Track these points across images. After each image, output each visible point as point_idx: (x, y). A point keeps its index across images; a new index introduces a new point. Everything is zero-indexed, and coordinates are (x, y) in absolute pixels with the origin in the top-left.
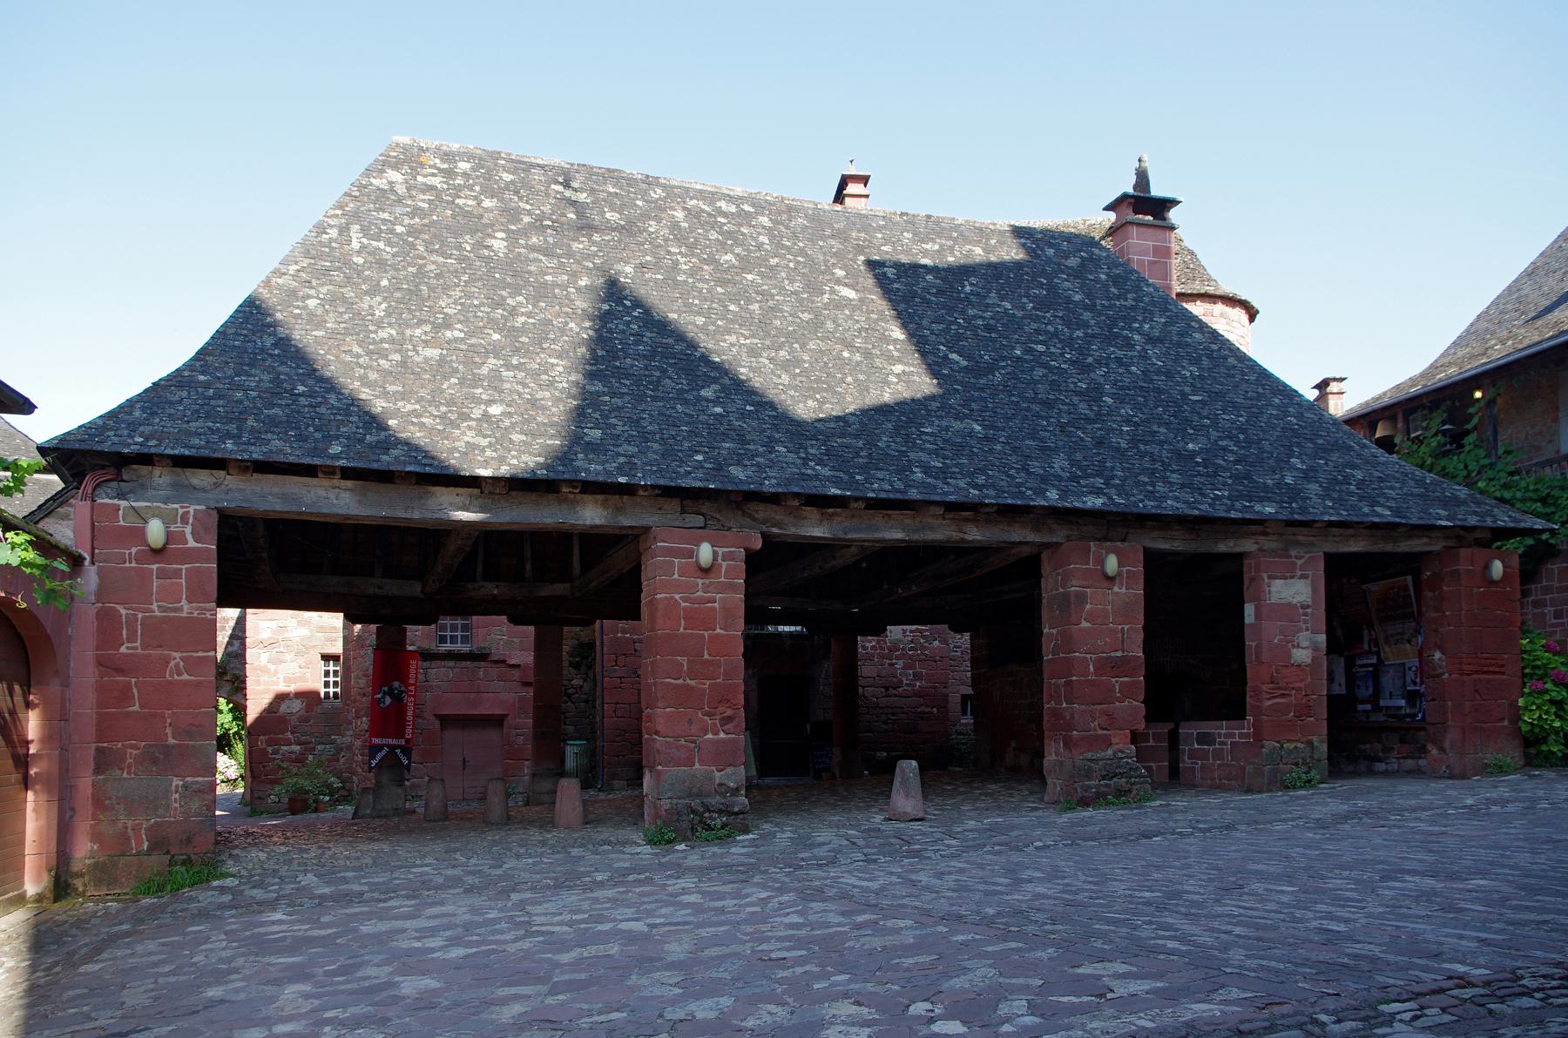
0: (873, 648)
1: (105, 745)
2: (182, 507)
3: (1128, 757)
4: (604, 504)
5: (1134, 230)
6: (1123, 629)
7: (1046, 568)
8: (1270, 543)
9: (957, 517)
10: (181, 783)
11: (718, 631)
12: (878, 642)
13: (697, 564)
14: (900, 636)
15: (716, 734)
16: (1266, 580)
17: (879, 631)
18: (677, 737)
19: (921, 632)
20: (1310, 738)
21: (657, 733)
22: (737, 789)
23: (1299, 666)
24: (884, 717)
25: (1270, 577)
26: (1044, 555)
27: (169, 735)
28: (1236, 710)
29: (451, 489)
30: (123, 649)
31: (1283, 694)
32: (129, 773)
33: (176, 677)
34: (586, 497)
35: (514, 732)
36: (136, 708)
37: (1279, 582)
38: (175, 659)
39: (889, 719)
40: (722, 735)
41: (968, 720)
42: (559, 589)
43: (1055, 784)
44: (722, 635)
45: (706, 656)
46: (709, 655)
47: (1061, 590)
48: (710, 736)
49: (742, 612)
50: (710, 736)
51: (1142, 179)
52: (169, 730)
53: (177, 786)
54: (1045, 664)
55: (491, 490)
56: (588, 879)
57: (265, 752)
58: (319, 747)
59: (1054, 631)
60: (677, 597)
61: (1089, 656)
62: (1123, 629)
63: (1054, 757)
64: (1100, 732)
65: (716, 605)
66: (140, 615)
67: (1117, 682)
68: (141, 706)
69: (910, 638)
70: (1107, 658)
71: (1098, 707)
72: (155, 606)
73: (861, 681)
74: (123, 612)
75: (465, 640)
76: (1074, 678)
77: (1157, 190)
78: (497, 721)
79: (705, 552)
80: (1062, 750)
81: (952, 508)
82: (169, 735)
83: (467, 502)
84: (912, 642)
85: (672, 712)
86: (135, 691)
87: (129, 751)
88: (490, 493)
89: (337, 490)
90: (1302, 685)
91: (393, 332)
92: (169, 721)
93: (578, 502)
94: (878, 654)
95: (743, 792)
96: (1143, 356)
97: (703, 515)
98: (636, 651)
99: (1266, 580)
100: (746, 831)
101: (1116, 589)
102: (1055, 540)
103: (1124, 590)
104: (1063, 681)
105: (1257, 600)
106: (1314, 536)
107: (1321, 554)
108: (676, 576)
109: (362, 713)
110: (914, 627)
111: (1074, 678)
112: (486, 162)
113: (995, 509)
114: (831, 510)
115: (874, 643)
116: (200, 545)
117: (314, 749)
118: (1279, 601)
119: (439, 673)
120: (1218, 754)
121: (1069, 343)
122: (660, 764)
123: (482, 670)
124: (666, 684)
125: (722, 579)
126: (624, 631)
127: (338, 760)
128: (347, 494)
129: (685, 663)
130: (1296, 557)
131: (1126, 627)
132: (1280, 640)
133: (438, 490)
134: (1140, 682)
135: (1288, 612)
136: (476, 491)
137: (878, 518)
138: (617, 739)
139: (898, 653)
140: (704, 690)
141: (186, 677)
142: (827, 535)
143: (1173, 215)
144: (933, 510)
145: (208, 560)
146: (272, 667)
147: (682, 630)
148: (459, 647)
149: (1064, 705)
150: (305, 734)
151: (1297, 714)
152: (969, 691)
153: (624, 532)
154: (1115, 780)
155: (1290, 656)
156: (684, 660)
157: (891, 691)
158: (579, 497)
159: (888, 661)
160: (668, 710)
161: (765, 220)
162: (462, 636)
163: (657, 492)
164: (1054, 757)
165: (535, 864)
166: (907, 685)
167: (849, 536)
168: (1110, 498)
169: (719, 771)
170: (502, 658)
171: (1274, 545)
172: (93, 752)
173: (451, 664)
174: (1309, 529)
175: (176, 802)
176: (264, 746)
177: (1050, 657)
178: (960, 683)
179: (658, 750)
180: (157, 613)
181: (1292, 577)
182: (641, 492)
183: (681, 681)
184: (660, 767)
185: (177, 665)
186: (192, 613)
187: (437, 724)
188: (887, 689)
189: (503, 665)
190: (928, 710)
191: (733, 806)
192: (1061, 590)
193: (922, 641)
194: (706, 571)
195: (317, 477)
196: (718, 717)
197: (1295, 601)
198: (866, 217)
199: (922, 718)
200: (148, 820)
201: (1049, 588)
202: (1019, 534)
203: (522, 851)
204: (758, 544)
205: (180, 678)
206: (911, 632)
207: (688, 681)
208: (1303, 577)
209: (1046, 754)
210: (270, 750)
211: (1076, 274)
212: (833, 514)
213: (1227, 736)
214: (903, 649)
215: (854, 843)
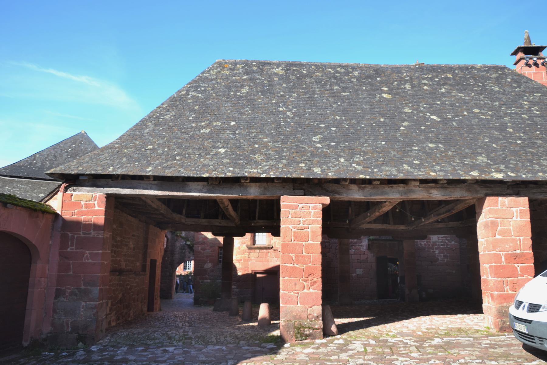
0: (425, 244)
1: (59, 287)
2: (94, 194)
4: (259, 187)
9: (426, 186)
10: (85, 304)
11: (310, 242)
12: (427, 242)
14: (437, 240)
19: (446, 237)
27: (82, 284)
30: (69, 250)
32: (66, 299)
33: (86, 261)
36: (71, 273)
38: (87, 253)
51: (529, 40)
52: (82, 282)
53: (83, 306)
55: (212, 182)
60: (290, 226)
61: (501, 253)
62: (520, 239)
65: (309, 230)
66: (76, 236)
67: (518, 267)
68: (73, 273)
69: (441, 240)
70: (511, 254)
71: (509, 279)
72: (81, 233)
74: (70, 235)
82: (82, 284)
83: (202, 188)
84: (442, 242)
85: (288, 279)
86: (71, 266)
87: (67, 290)
88: (212, 184)
89: (151, 185)
92: (82, 278)
93: (248, 186)
94: (427, 247)
96: (529, 110)
97: (304, 190)
103: (519, 219)
108: (290, 217)
110: (443, 236)
112: (247, 64)
113: (445, 182)
115: (425, 243)
116: (100, 208)
121: (491, 108)
129: (294, 257)
131: (522, 238)
134: (531, 266)
136: (206, 183)
137: (387, 189)
141: (90, 261)
144: (413, 183)
146: (202, 252)
158: (248, 184)
159: (432, 250)
161: (356, 73)
166: (441, 260)
168: (507, 174)
172: (54, 290)
173: (258, 251)
175: (82, 312)
180: (82, 235)
182: (276, 181)
183: (292, 265)
185: (87, 256)
186: (94, 235)
191: (315, 324)
193: (447, 241)
195: (144, 180)
198: (400, 68)
200: (72, 319)
202: (457, 194)
205: (88, 261)
206: (441, 238)
207: (295, 265)
211: (497, 81)
214: (438, 245)
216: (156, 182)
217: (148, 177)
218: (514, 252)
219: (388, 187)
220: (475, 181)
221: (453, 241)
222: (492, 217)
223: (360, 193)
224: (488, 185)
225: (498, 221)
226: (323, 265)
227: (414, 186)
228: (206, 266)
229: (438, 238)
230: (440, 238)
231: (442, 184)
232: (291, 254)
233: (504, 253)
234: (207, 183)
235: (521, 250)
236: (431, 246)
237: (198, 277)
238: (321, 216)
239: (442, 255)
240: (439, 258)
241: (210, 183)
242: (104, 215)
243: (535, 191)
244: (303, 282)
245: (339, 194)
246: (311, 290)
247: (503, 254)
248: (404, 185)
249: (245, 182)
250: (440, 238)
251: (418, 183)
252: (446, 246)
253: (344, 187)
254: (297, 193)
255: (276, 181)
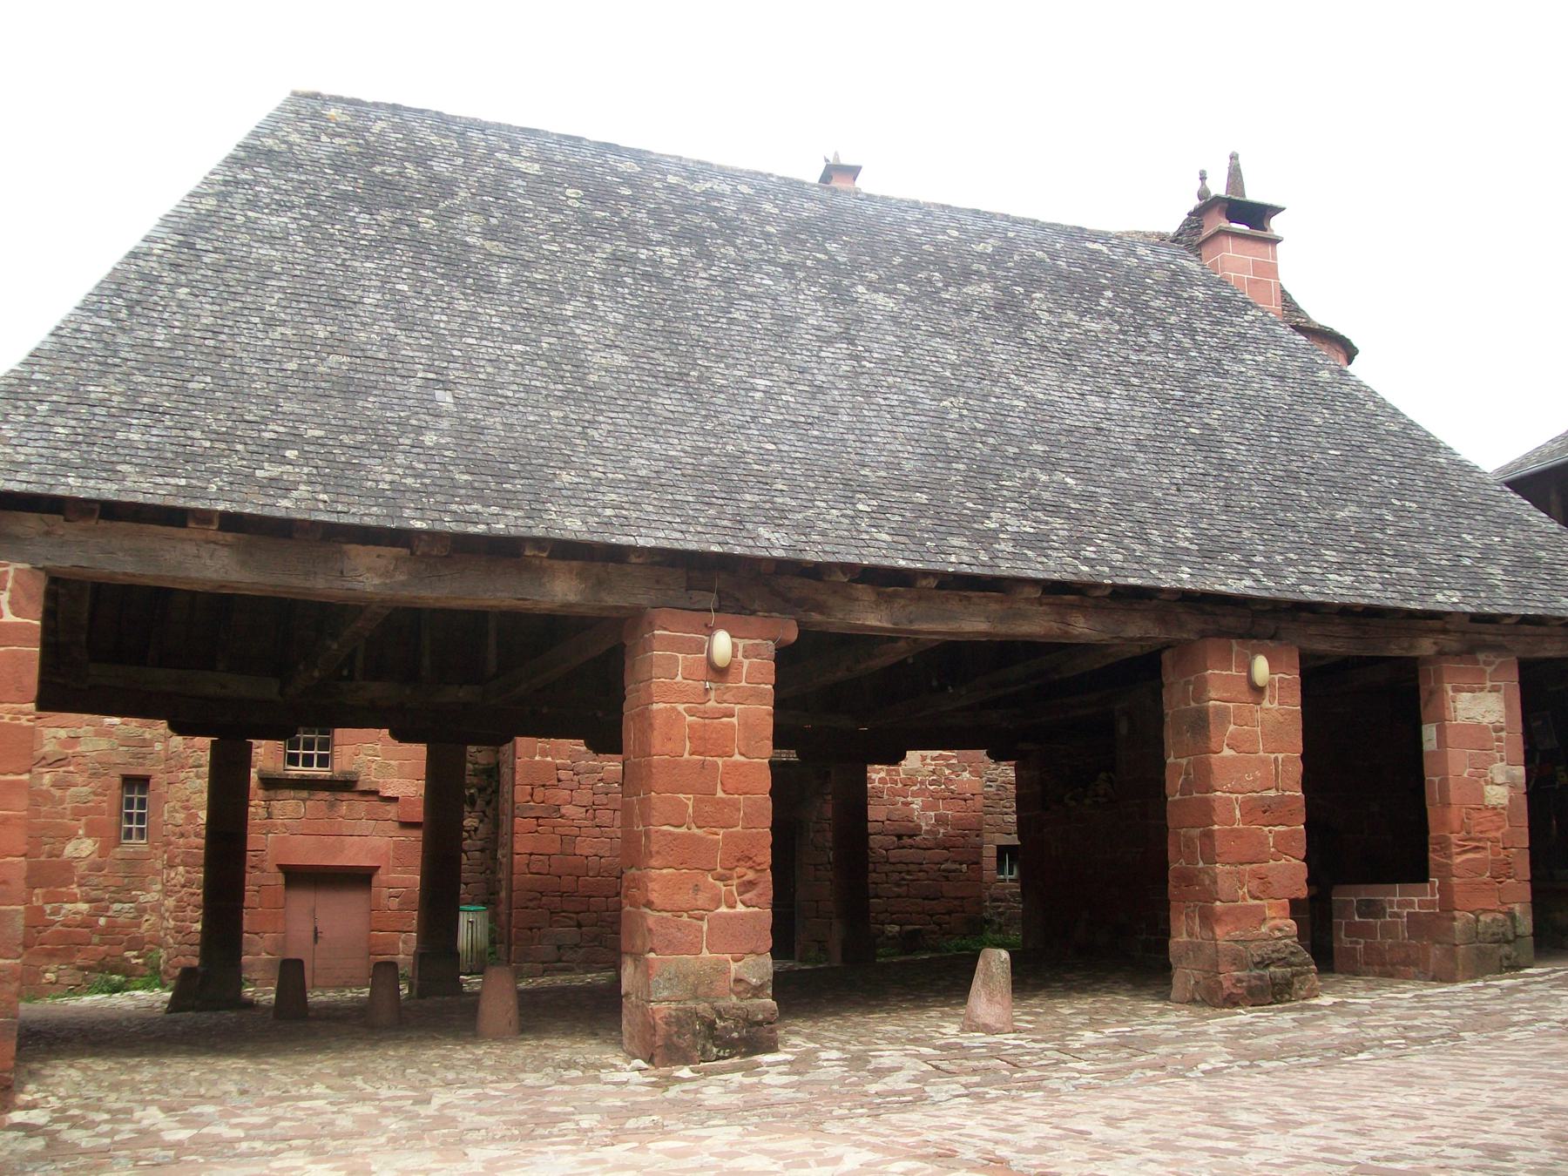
0: (882, 780)
3: (1286, 937)
5: (1230, 243)
6: (1276, 759)
7: (1169, 676)
8: (1450, 642)
11: (737, 757)
12: (888, 773)
13: (710, 661)
14: (918, 764)
15: (732, 906)
16: (1451, 693)
17: (895, 758)
18: (677, 912)
20: (1511, 906)
21: (649, 904)
22: (762, 987)
23: (1494, 808)
24: (895, 876)
25: (1457, 690)
26: (1166, 656)
28: (1417, 871)
29: (371, 547)
31: (1477, 847)
34: (557, 564)
35: (386, 892)
37: (1466, 696)
39: (904, 879)
40: (740, 908)
41: (1010, 876)
42: (463, 693)
43: (1185, 976)
44: (743, 764)
45: (720, 794)
46: (724, 791)
47: (1193, 704)
48: (723, 909)
49: (769, 731)
50: (723, 909)
54: (1168, 804)
56: (571, 1125)
57: (41, 910)
58: (117, 906)
59: (1184, 761)
60: (681, 707)
62: (1276, 759)
63: (1184, 938)
64: (1252, 902)
65: (734, 720)
69: (931, 768)
71: (1248, 867)
73: (871, 827)
75: (324, 761)
76: (1216, 827)
77: (1255, 193)
78: (359, 878)
79: (722, 644)
80: (1197, 928)
81: (1054, 590)
84: (934, 772)
85: (672, 875)
89: (212, 546)
90: (1498, 835)
91: (289, 332)
95: (770, 991)
98: (559, 780)
99: (1451, 693)
100: (772, 1048)
101: (1266, 704)
102: (1185, 636)
103: (1276, 705)
104: (1198, 830)
105: (1440, 721)
106: (1503, 635)
107: (1514, 658)
108: (679, 678)
109: (178, 860)
110: (936, 753)
111: (1216, 827)
114: (891, 589)
116: (19, 620)
117: (107, 909)
118: (1468, 722)
119: (289, 807)
120: (1388, 930)
122: (652, 950)
123: (347, 806)
124: (665, 834)
125: (743, 684)
126: (544, 753)
127: (139, 926)
128: (225, 552)
129: (690, 804)
130: (1485, 663)
131: (1280, 756)
132: (1471, 775)
133: (353, 549)
135: (1478, 735)
136: (404, 552)
138: (531, 904)
139: (915, 788)
140: (717, 842)
142: (885, 625)
143: (1276, 225)
145: (27, 643)
147: (686, 756)
148: (315, 771)
149: (1201, 864)
150: (96, 887)
151: (1495, 874)
152: (1014, 840)
153: (605, 614)
154: (1272, 969)
155: (1482, 796)
156: (688, 799)
157: (906, 841)
158: (546, 563)
159: (903, 799)
160: (665, 871)
162: (319, 756)
163: (657, 559)
164: (1184, 938)
165: (477, 1097)
167: (915, 627)
169: (736, 960)
170: (373, 788)
171: (1455, 646)
174: (1496, 626)
176: (40, 903)
177: (1178, 796)
178: (1003, 828)
179: (650, 930)
181: (1482, 690)
182: (634, 560)
183: (683, 830)
184: (652, 955)
187: (281, 879)
188: (900, 837)
189: (375, 798)
190: (957, 866)
192: (1193, 704)
194: (719, 673)
196: (735, 882)
197: (1485, 721)
199: (947, 879)
201: (1174, 702)
203: (451, 1075)
204: (792, 635)
206: (933, 759)
207: (695, 830)
208: (1494, 689)
209: (1173, 933)
210: (48, 908)
212: (896, 595)
213: (1400, 905)
214: (922, 783)
215: (937, 1067)
216: (229, 537)
217: (204, 517)
218: (1264, 794)
219: (957, 598)
220: (1179, 596)
221: (965, 770)
222: (1216, 697)
223: (881, 611)
224: (1208, 608)
225: (1229, 708)
226: (776, 828)
227: (1027, 600)
228: (70, 850)
229: (924, 758)
230: (929, 761)
231: (1097, 597)
232: (681, 796)
233: (1240, 796)
234: (409, 552)
235: (1277, 790)
236: (900, 785)
237: (37, 891)
238: (772, 678)
239: (933, 814)
240: (923, 824)
241: (418, 553)
242: (38, 644)
243: (1312, 630)
244: (717, 882)
245: (822, 613)
246: (740, 908)
247: (1237, 799)
248: (1000, 594)
249: (534, 556)
250: (929, 761)
251: (1036, 593)
252: (943, 787)
253: (835, 592)
254: (699, 601)
255: (634, 560)
